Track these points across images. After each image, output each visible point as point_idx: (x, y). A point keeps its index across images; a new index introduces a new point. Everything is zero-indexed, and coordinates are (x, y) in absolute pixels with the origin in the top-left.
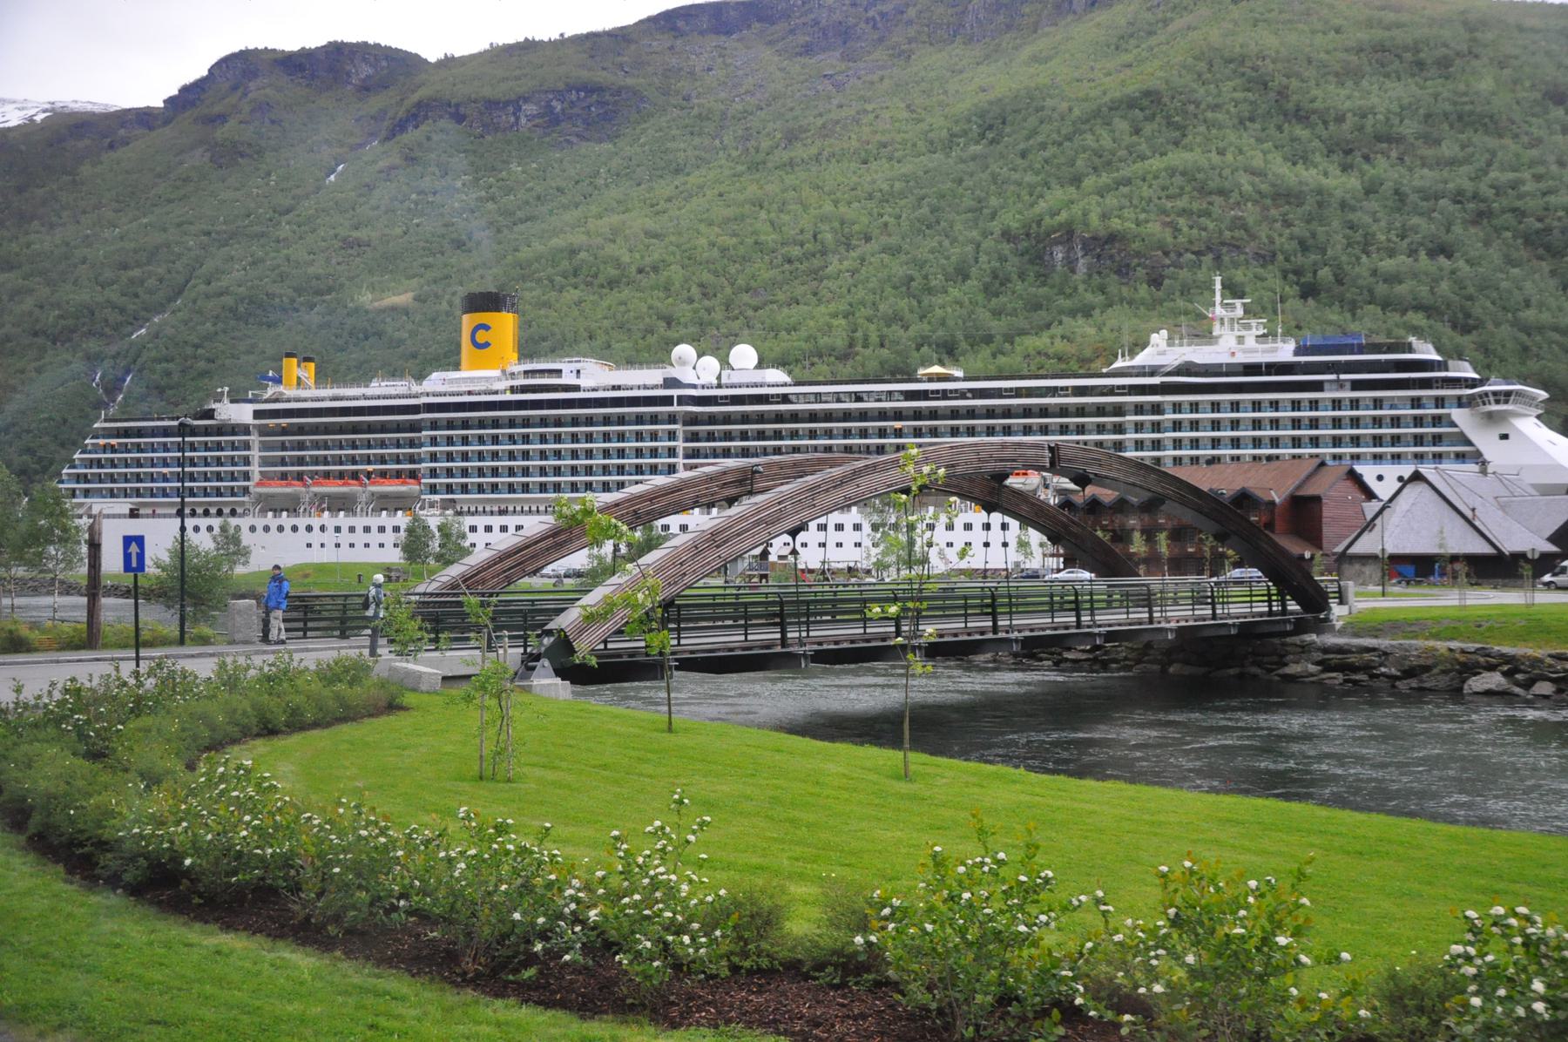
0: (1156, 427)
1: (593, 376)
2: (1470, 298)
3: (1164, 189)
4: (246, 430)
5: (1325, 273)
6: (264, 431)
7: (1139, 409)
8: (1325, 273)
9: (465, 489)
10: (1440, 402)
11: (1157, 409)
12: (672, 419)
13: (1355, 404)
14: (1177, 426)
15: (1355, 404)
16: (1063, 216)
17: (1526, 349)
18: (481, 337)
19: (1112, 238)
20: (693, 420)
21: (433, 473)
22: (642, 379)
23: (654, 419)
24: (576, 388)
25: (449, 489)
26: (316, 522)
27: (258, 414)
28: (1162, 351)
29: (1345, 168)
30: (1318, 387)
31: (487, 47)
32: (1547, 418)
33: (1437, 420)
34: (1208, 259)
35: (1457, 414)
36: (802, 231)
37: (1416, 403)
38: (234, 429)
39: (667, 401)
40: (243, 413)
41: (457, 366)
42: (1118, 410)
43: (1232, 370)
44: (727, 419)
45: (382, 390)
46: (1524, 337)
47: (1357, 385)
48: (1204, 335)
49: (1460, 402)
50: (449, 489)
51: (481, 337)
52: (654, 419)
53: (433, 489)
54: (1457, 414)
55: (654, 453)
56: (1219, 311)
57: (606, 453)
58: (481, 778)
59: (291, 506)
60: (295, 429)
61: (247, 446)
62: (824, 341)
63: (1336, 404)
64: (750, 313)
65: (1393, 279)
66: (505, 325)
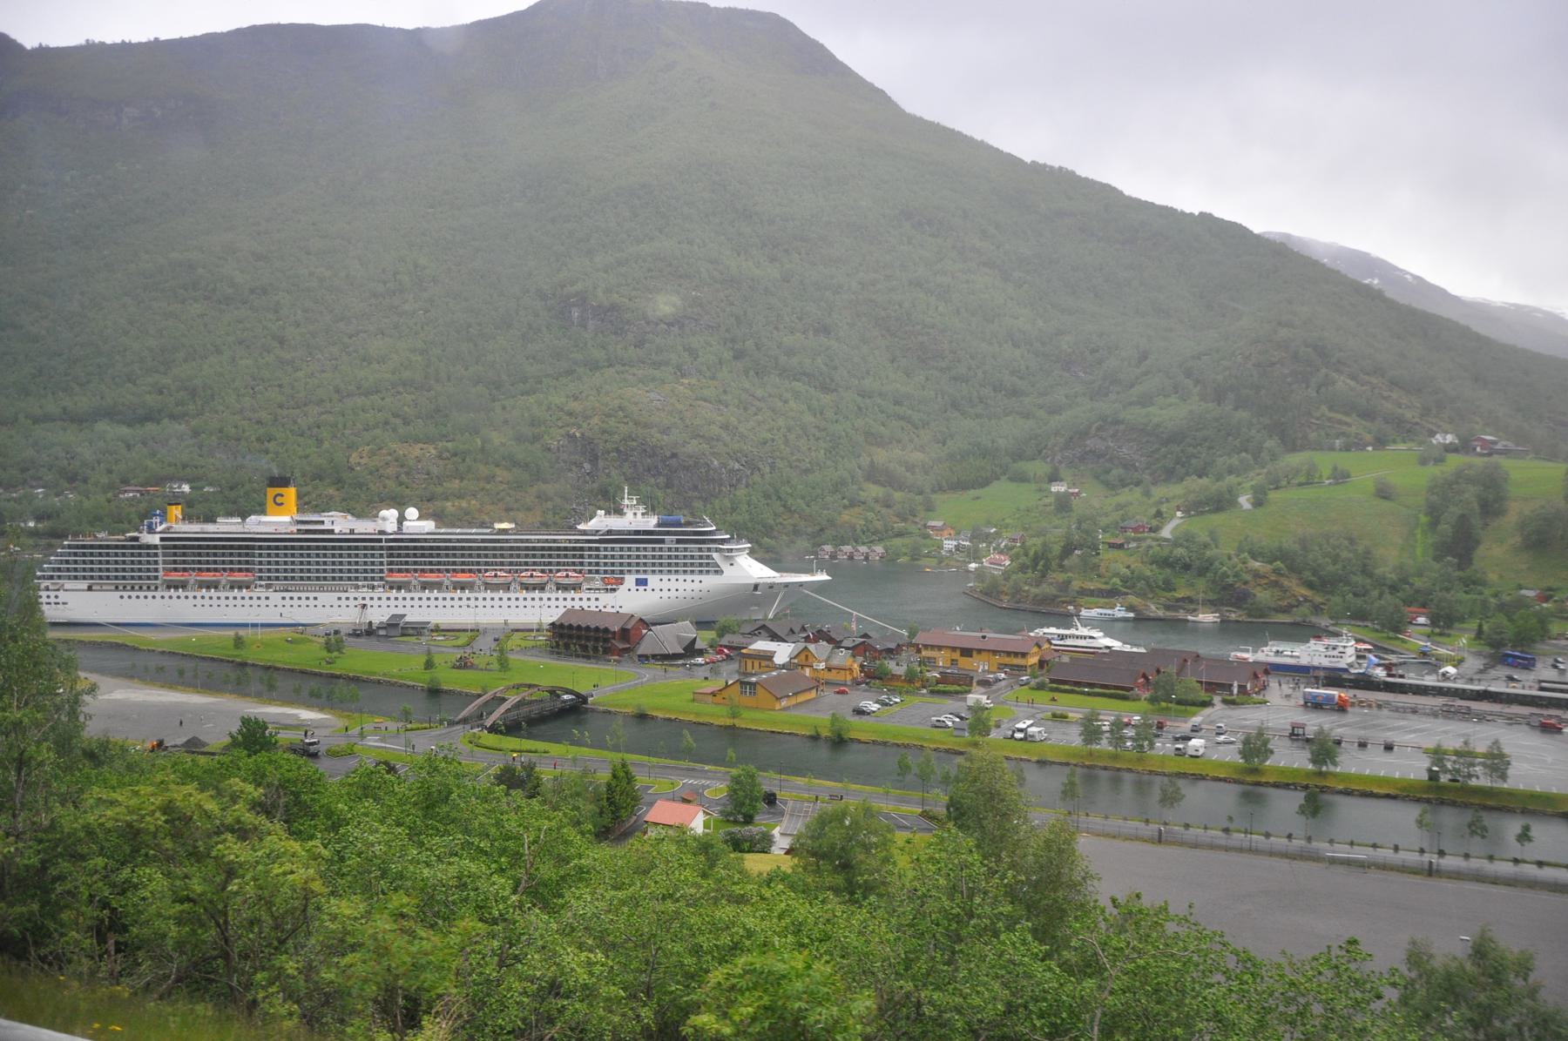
0: (597, 557)
1: (340, 523)
2: (836, 368)
3: (650, 270)
4: (156, 547)
5: (750, 344)
6: (164, 547)
7: (590, 549)
8: (750, 344)
9: (277, 578)
10: (709, 550)
11: (597, 549)
12: (381, 548)
13: (677, 550)
14: (606, 557)
15: (677, 550)
16: (579, 287)
17: (860, 409)
18: (279, 500)
19: (614, 308)
20: (391, 548)
21: (261, 571)
22: (364, 527)
23: (373, 548)
24: (332, 532)
25: (269, 578)
26: (199, 594)
27: (162, 539)
28: (601, 521)
29: (773, 260)
30: (662, 541)
31: (83, 42)
32: (752, 553)
33: (708, 557)
34: (675, 329)
35: (715, 555)
36: (384, 271)
37: (700, 550)
38: (149, 547)
39: (380, 540)
40: (155, 539)
41: (263, 512)
42: (582, 549)
43: (629, 533)
44: (407, 548)
45: (227, 526)
46: (859, 399)
47: (678, 541)
48: (619, 512)
49: (717, 550)
50: (269, 578)
51: (279, 500)
52: (373, 548)
53: (261, 578)
54: (715, 555)
55: (373, 563)
56: (626, 502)
57: (349, 563)
58: (1160, 841)
59: (183, 585)
60: (177, 547)
61: (156, 555)
62: (407, 374)
63: (670, 549)
64: (346, 340)
65: (790, 352)
66: (291, 492)
